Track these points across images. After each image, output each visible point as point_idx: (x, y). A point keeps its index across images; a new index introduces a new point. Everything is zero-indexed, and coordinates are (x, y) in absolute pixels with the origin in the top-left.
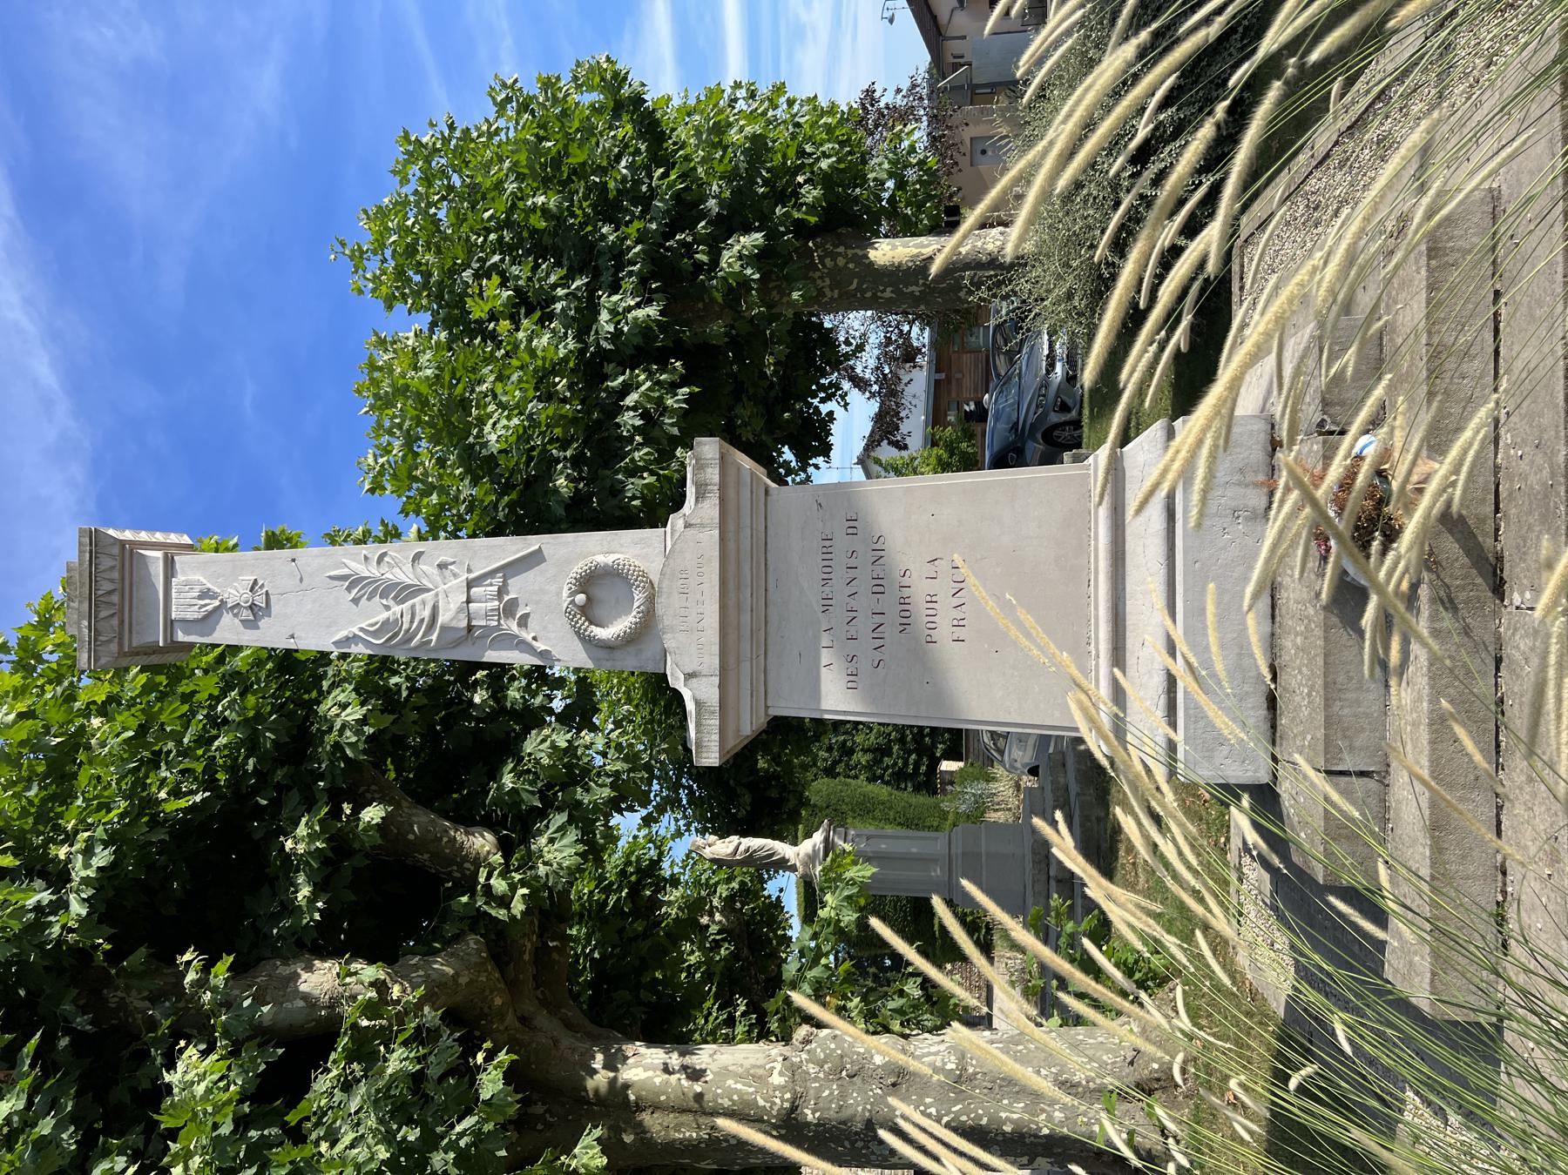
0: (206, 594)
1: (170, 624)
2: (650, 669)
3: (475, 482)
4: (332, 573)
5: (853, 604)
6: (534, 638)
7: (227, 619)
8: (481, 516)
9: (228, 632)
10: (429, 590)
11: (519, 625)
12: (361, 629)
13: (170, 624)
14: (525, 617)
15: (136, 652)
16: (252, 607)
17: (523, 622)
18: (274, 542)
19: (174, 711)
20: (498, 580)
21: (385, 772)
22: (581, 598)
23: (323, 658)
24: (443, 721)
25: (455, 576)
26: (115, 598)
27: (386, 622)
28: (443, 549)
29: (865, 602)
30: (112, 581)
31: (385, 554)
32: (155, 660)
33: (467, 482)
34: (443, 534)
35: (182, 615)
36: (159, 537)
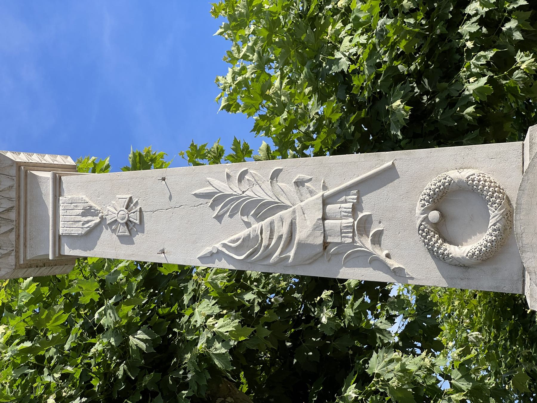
0: (88, 211)
1: (58, 239)
2: (507, 289)
3: (322, 100)
4: (197, 191)
6: (388, 256)
7: (106, 234)
8: (328, 134)
9: (106, 246)
10: (286, 207)
11: (373, 242)
12: (224, 245)
13: (58, 239)
14: (378, 235)
15: (31, 265)
16: (128, 223)
17: (377, 239)
18: (142, 163)
19: (57, 319)
20: (352, 197)
21: (239, 384)
22: (434, 215)
23: (185, 272)
24: (292, 338)
25: (311, 193)
26: (13, 215)
27: (247, 239)
28: (295, 167)
30: (10, 199)
31: (245, 172)
32: (45, 272)
33: (314, 99)
34: (291, 152)
35: (68, 231)
36: (48, 159)
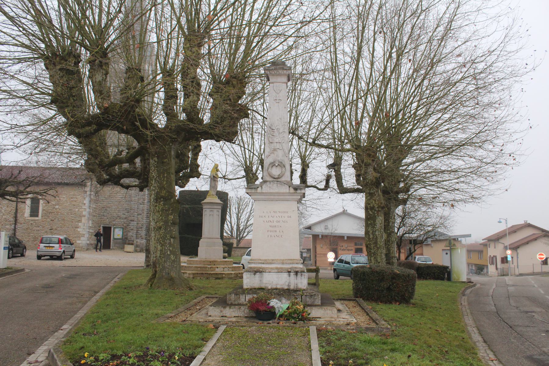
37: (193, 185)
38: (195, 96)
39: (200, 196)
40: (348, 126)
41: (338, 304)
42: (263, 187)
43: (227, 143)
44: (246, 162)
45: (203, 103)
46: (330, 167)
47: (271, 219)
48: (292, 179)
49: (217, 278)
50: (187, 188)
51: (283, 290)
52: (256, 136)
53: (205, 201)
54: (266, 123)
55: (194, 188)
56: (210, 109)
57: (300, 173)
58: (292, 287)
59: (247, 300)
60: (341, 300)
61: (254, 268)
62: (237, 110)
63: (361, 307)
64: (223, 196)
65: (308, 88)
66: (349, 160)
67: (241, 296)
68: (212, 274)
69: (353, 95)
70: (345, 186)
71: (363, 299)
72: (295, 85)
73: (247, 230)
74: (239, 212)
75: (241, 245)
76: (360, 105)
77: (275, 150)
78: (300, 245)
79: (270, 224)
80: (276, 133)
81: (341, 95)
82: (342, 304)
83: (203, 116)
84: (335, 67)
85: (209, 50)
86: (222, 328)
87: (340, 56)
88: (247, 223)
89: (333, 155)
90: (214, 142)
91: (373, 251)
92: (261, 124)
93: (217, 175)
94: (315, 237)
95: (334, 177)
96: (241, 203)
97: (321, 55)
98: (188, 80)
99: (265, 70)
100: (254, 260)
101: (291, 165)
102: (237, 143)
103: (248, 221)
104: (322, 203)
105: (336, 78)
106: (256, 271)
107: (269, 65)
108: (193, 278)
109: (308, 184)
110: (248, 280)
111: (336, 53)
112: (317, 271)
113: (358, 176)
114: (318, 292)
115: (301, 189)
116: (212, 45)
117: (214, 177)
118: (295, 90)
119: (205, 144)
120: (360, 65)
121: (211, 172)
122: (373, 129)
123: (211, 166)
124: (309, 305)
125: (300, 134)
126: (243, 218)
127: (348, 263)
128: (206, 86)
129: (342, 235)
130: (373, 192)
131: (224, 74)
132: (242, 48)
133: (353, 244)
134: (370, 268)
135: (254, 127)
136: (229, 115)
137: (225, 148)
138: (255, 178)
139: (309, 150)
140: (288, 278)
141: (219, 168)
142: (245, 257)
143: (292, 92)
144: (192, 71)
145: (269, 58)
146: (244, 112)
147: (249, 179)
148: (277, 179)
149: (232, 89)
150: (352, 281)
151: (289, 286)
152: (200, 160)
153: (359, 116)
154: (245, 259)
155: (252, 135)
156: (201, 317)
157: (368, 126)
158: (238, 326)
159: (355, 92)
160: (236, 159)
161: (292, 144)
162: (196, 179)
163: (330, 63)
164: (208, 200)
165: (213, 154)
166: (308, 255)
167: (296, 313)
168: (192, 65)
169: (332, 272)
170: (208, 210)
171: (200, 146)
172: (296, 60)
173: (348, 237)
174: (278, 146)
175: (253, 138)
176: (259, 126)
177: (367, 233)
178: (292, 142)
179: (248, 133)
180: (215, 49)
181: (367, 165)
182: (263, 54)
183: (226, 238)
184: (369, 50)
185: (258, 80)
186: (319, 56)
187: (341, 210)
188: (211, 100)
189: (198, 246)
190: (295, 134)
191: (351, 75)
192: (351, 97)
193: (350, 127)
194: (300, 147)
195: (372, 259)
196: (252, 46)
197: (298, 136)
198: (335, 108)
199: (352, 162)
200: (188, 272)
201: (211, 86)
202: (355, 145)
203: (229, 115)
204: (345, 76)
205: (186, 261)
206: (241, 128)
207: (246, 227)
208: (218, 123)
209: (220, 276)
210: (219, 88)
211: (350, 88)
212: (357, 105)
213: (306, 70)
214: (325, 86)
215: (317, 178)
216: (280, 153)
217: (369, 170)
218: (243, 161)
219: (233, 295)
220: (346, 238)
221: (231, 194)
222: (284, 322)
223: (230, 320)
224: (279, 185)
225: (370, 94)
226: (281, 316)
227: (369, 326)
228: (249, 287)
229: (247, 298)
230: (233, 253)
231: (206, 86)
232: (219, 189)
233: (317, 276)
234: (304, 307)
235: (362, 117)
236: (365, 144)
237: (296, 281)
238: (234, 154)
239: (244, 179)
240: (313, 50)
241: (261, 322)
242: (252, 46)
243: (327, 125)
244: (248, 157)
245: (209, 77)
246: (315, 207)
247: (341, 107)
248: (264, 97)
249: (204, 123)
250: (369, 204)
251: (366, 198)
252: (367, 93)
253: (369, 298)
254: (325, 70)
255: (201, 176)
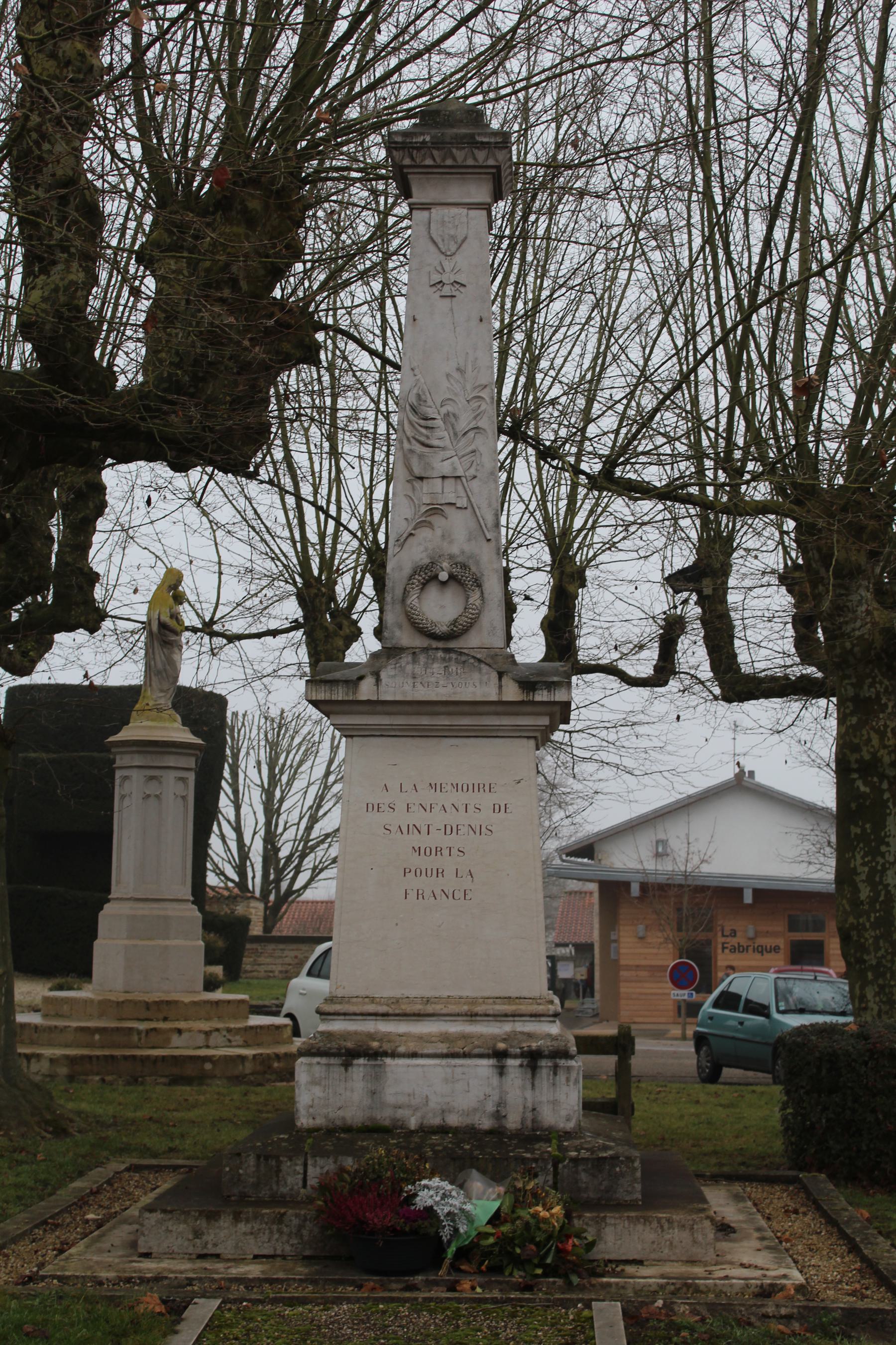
5: (437, 809)
26: (449, 162)
29: (438, 819)
37: (72, 660)
38: (75, 265)
39: (98, 709)
40: (761, 401)
41: (720, 1201)
42: (383, 675)
43: (219, 475)
44: (304, 561)
45: (112, 294)
46: (676, 581)
47: (418, 817)
48: (509, 638)
49: (176, 1080)
50: (40, 676)
51: (471, 1132)
52: (349, 447)
53: (124, 735)
54: (396, 387)
55: (73, 677)
56: (144, 326)
57: (544, 611)
58: (513, 1122)
59: (312, 1182)
60: (731, 1178)
61: (345, 1036)
62: (268, 331)
63: (824, 1214)
64: (205, 712)
65: (578, 233)
66: (762, 552)
67: (286, 1165)
68: (156, 1060)
69: (785, 261)
70: (745, 669)
71: (832, 1177)
72: (525, 218)
73: (309, 863)
74: (273, 780)
75: (285, 927)
76: (819, 304)
77: (435, 510)
78: (547, 928)
79: (415, 839)
80: (441, 436)
81: (729, 261)
82: (737, 1198)
83: (113, 356)
84: (706, 132)
85: (138, 51)
86: (203, 1310)
87: (728, 80)
88: (309, 828)
89: (690, 527)
90: (162, 470)
91: (871, 959)
92: (373, 390)
93: (176, 617)
94: (613, 891)
95: (698, 625)
96: (285, 743)
97: (642, 78)
98: (40, 193)
99: (390, 145)
100: (342, 1000)
101: (506, 575)
102: (263, 474)
103: (314, 819)
104: (644, 743)
105: (707, 180)
106: (349, 1053)
107: (406, 124)
108: (71, 1078)
109: (582, 656)
110: (317, 1091)
111: (711, 67)
112: (621, 1045)
113: (803, 623)
114: (629, 1143)
115: (551, 686)
116: (150, 28)
117: (163, 626)
118: (525, 239)
119: (115, 478)
120: (822, 121)
121: (152, 603)
122: (876, 409)
123: (151, 580)
124: (589, 1205)
125: (547, 437)
126: (293, 809)
127: (761, 1010)
128: (123, 218)
129: (738, 883)
130: (872, 693)
131: (205, 163)
132: (287, 45)
133: (780, 926)
134: (862, 1036)
135: (341, 403)
136: (228, 351)
137: (213, 497)
138: (346, 631)
139: (587, 506)
140: (495, 1081)
141: (186, 586)
142: (302, 982)
143: (512, 247)
144: (61, 147)
145: (407, 90)
146: (296, 337)
147: (320, 634)
148: (445, 641)
149: (240, 228)
150: (777, 1090)
151: (498, 1116)
152: (101, 554)
153: (814, 349)
154: (304, 991)
155: (332, 439)
156: (107, 1258)
157: (850, 399)
158: (275, 1301)
159: (795, 245)
160: (262, 547)
161: (510, 478)
162: (81, 635)
163: (683, 113)
164: (136, 730)
165: (159, 526)
166: (581, 974)
167: (532, 1240)
168: (59, 123)
169: (689, 1047)
170: (134, 774)
171: (101, 489)
172: (527, 99)
173: (758, 893)
174: (450, 492)
175: (339, 460)
176: (365, 402)
177: (844, 874)
178: (511, 471)
179: (314, 430)
180: (163, 48)
181: (848, 575)
182: (380, 71)
183: (219, 898)
184: (862, 51)
185: (359, 193)
186: (632, 80)
187: (728, 773)
188: (150, 284)
189: (95, 936)
190: (525, 438)
191: (778, 168)
192: (777, 268)
193: (770, 402)
194: (544, 493)
195: (870, 992)
196: (334, 38)
197: (536, 443)
198: (702, 321)
199: (775, 560)
200: (48, 1052)
201: (148, 218)
202: (794, 485)
203: (228, 351)
204: (748, 175)
205: (38, 1000)
206: (281, 410)
207: (306, 847)
208: (179, 389)
209: (189, 1070)
210: (183, 227)
211: (770, 228)
212: (801, 307)
213: (575, 145)
214: (658, 216)
215: (619, 632)
216: (458, 524)
217: (855, 598)
218: (291, 553)
219: (252, 1161)
220: (748, 898)
221: (240, 703)
222: (479, 1279)
223: (236, 1271)
224: (453, 668)
225: (864, 255)
226: (463, 1253)
227: (861, 1305)
228: (320, 1121)
229: (313, 1172)
230: (247, 963)
231: (123, 218)
232: (186, 679)
233: (623, 1074)
234: (568, 1215)
235: (827, 356)
236: (840, 480)
237: (529, 1094)
238: (254, 523)
239: (299, 634)
240: (607, 52)
241: (372, 1281)
242: (334, 38)
243: (667, 397)
244: (313, 537)
245: (138, 176)
246: (615, 759)
247: (731, 313)
248: (385, 272)
249: (122, 382)
250: (856, 749)
251: (841, 721)
252: (848, 251)
253: (856, 1174)
254: (657, 147)
255: (107, 624)
